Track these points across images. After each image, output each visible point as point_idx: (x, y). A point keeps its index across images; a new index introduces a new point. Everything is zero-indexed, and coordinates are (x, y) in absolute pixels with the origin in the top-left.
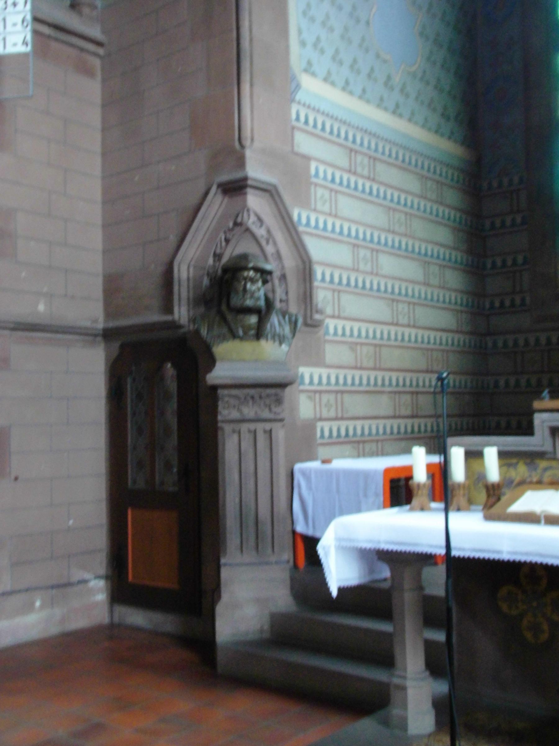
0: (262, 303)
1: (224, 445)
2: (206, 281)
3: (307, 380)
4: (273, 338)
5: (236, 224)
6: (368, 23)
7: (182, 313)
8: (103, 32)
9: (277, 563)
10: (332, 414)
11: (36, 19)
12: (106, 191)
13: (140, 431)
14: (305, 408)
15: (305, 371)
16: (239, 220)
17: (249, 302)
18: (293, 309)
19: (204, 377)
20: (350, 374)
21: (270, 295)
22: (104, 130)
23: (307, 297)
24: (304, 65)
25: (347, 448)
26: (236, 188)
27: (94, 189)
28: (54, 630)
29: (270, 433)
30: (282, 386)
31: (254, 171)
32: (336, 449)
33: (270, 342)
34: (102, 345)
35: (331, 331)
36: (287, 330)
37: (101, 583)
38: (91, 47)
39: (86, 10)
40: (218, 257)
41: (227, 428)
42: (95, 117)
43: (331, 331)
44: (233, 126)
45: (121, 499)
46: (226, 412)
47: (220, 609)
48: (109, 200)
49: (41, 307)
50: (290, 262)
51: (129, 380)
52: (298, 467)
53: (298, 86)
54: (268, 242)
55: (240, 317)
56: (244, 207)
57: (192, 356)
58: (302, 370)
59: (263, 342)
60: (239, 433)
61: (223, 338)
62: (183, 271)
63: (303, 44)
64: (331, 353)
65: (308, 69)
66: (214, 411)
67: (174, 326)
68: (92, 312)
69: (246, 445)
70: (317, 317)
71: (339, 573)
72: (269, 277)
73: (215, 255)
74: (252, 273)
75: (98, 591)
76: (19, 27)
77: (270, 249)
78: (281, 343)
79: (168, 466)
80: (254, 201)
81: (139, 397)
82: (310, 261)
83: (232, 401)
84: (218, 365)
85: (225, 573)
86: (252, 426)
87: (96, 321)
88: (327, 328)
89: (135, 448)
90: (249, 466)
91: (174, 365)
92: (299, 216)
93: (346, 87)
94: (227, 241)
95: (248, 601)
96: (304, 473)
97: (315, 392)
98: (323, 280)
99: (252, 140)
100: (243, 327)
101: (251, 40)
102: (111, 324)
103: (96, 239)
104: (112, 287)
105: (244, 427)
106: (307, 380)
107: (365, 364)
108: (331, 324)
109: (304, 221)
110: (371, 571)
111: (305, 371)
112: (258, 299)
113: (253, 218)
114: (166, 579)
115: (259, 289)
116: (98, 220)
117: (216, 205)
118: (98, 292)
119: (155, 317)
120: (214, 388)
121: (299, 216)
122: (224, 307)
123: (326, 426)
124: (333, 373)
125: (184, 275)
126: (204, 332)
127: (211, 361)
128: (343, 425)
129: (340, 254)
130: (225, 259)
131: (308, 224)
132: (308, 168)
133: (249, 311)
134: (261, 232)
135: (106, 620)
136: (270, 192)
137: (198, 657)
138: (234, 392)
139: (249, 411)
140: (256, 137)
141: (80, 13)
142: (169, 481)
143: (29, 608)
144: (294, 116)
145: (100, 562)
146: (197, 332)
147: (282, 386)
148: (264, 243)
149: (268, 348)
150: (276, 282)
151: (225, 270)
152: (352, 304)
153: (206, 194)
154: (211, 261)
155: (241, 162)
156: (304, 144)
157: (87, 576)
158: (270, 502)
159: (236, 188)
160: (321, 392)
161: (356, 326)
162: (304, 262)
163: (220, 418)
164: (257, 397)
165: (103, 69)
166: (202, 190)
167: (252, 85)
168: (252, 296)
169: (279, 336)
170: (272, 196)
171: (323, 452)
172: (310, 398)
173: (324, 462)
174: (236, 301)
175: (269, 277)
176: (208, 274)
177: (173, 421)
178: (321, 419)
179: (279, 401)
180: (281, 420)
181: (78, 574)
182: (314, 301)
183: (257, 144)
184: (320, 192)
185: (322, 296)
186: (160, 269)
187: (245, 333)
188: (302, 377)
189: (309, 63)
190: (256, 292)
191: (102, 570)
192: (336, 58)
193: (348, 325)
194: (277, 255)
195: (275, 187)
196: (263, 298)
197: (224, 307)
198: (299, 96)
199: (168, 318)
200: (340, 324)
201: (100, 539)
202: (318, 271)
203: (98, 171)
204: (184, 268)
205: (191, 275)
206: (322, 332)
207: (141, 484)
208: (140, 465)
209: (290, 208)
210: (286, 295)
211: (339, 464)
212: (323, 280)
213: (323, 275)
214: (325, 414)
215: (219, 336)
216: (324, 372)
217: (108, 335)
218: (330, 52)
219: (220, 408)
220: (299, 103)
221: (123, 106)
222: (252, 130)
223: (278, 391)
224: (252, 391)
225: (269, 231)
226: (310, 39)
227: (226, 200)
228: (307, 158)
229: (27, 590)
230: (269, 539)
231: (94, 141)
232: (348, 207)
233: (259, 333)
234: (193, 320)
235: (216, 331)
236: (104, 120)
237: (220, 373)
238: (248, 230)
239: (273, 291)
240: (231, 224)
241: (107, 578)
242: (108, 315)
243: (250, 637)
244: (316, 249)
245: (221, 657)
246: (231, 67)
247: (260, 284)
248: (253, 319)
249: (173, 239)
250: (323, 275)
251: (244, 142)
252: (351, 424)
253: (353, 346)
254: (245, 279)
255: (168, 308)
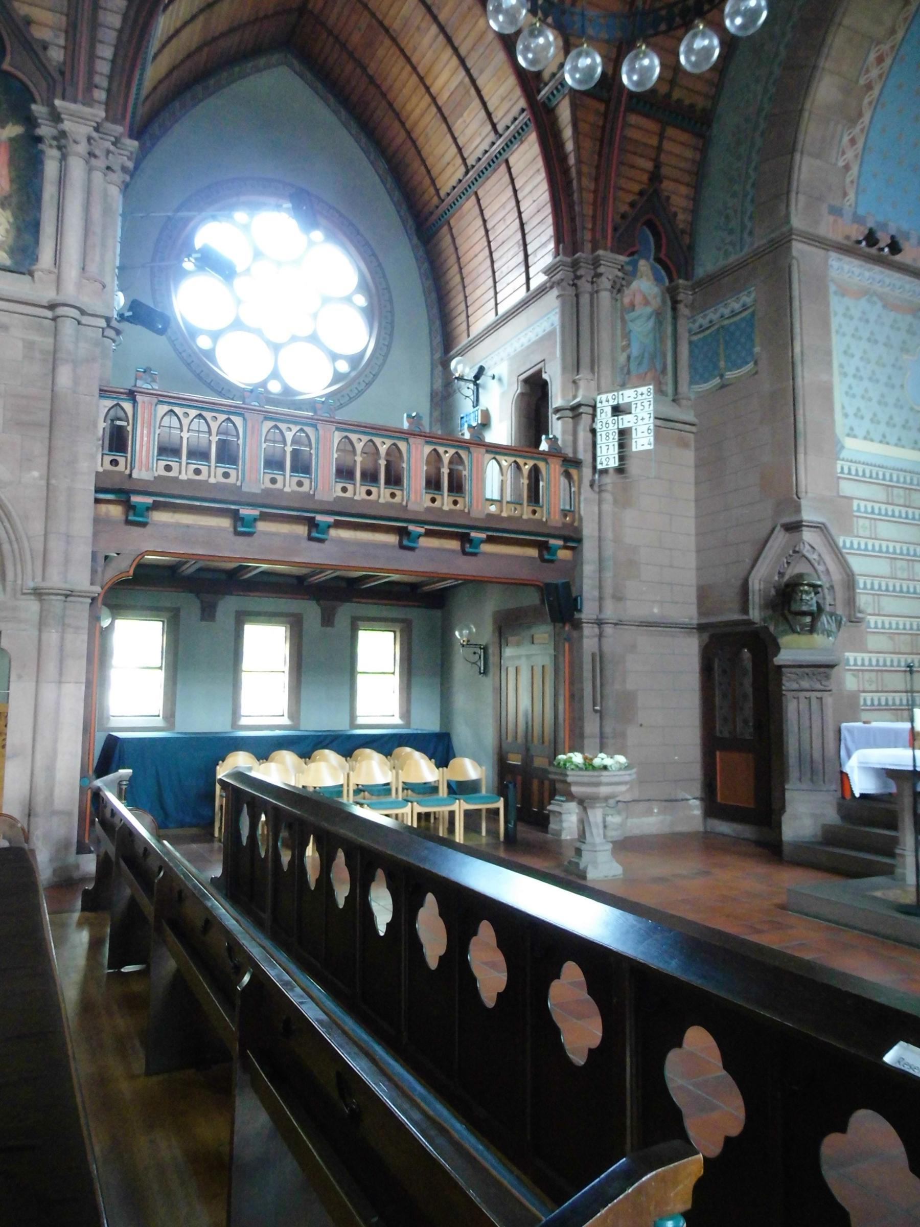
0: (815, 608)
1: (787, 707)
2: (773, 592)
3: (852, 662)
4: (823, 633)
5: (795, 552)
6: (902, 386)
7: (755, 614)
8: (696, 416)
9: (827, 791)
10: (873, 688)
11: (656, 418)
12: (698, 527)
13: (724, 696)
14: (851, 683)
15: (850, 656)
16: (797, 549)
17: (805, 608)
18: (839, 612)
19: (772, 661)
20: (889, 657)
21: (821, 601)
22: (697, 483)
23: (851, 601)
24: (847, 430)
25: (887, 714)
26: (795, 527)
27: (689, 525)
28: (666, 830)
29: (821, 699)
30: (831, 666)
31: (807, 515)
32: (876, 714)
33: (821, 636)
34: (696, 636)
35: (872, 625)
36: (834, 626)
37: (697, 803)
38: (687, 427)
39: (684, 402)
40: (781, 574)
41: (789, 695)
42: (690, 474)
43: (872, 625)
44: (792, 485)
45: (712, 743)
46: (788, 684)
47: (785, 819)
48: (701, 533)
49: (656, 610)
50: (837, 576)
51: (716, 661)
52: (844, 725)
53: (843, 447)
54: (819, 564)
55: (799, 617)
56: (801, 540)
57: (762, 644)
58: (847, 654)
59: (815, 636)
60: (798, 698)
61: (785, 633)
62: (756, 585)
63: (846, 415)
64: (872, 642)
65: (851, 434)
66: (779, 684)
67: (750, 623)
68: (689, 613)
69: (803, 705)
70: (859, 615)
71: (862, 784)
72: (820, 589)
73: (779, 573)
74: (806, 588)
75: (695, 808)
76: (646, 434)
77: (820, 568)
78: (828, 636)
79: (745, 722)
80: (808, 535)
81: (724, 672)
82: (853, 575)
83: (793, 676)
84: (783, 652)
85: (788, 795)
86: (808, 694)
87: (691, 618)
88: (869, 622)
89: (721, 708)
90: (805, 722)
91: (749, 650)
92: (844, 542)
93: (883, 440)
94: (788, 563)
95: (804, 815)
96: (850, 730)
97: (858, 670)
98: (865, 588)
99: (806, 492)
100: (800, 625)
101: (805, 423)
102: (704, 621)
103: (691, 560)
104: (703, 594)
105: (802, 695)
106: (852, 662)
107: (903, 650)
108: (872, 620)
109: (848, 545)
110: (885, 785)
111: (850, 656)
112: (811, 605)
113: (807, 547)
114: (745, 798)
115: (812, 599)
116: (693, 546)
117: (780, 539)
118: (693, 598)
119: (736, 617)
120: (780, 667)
121: (844, 542)
122: (786, 612)
123: (869, 696)
124: (874, 657)
125: (757, 587)
126: (772, 628)
127: (777, 649)
128: (883, 696)
129: (881, 567)
130: (786, 577)
131: (852, 547)
132: (852, 505)
133: (805, 614)
134: (813, 557)
135: (701, 829)
136: (821, 528)
137: (772, 849)
138: (794, 670)
139: (805, 684)
140: (809, 491)
141: (679, 405)
142: (747, 733)
143: (649, 813)
144: (839, 470)
145: (697, 789)
146: (767, 628)
147: (831, 666)
148: (816, 564)
149: (818, 639)
150: (826, 591)
151: (787, 585)
152: (890, 604)
153: (774, 529)
154: (776, 578)
155: (798, 509)
156: (847, 488)
157: (689, 797)
158: (581, 328)
159: (795, 527)
160: (862, 671)
161: (894, 620)
162: (848, 575)
163: (784, 688)
164: (810, 674)
165: (696, 441)
166: (770, 528)
167: (805, 454)
168: (807, 604)
169: (827, 631)
170: (822, 530)
171: (865, 716)
172: (854, 675)
173: (864, 723)
174: (795, 607)
175: (820, 589)
176: (774, 587)
177: (749, 690)
178: (864, 692)
179: (828, 677)
180: (830, 691)
181: (681, 795)
182: (857, 604)
183: (810, 495)
184: (861, 522)
185: (863, 600)
186: (739, 583)
187: (801, 629)
188: (848, 660)
189: (852, 429)
190: (810, 601)
191: (698, 793)
192: (874, 420)
193: (887, 620)
194: (826, 571)
195: (823, 524)
196: (815, 605)
197: (786, 612)
198: (844, 454)
199: (745, 617)
200: (880, 619)
201: (696, 771)
202: (861, 581)
203: (692, 512)
204: (757, 582)
205: (762, 587)
206: (863, 625)
207: (726, 734)
208: (725, 720)
209: (835, 537)
210: (834, 601)
211: (874, 724)
212: (865, 588)
213: (865, 583)
214: (868, 688)
215: (782, 632)
216: (866, 656)
217: (701, 628)
218: (868, 416)
219: (784, 682)
220: (843, 460)
221: (711, 469)
222: (806, 486)
223: (826, 670)
224: (806, 670)
225: (820, 555)
226: (851, 411)
227: (788, 535)
228: (851, 499)
229: (649, 800)
230: (821, 775)
231: (689, 492)
232: (885, 530)
233: (812, 629)
234: (764, 620)
235: (781, 628)
236: (696, 477)
237: (784, 657)
238: (804, 556)
239: (824, 598)
240: (791, 552)
241: (702, 799)
242: (701, 614)
243: (807, 840)
244: (857, 564)
245: (786, 849)
246: (790, 440)
247: (813, 595)
248: (808, 619)
249: (748, 561)
250: (865, 583)
251: (800, 495)
252: (890, 696)
253: (891, 636)
254: (801, 591)
255: (745, 609)
